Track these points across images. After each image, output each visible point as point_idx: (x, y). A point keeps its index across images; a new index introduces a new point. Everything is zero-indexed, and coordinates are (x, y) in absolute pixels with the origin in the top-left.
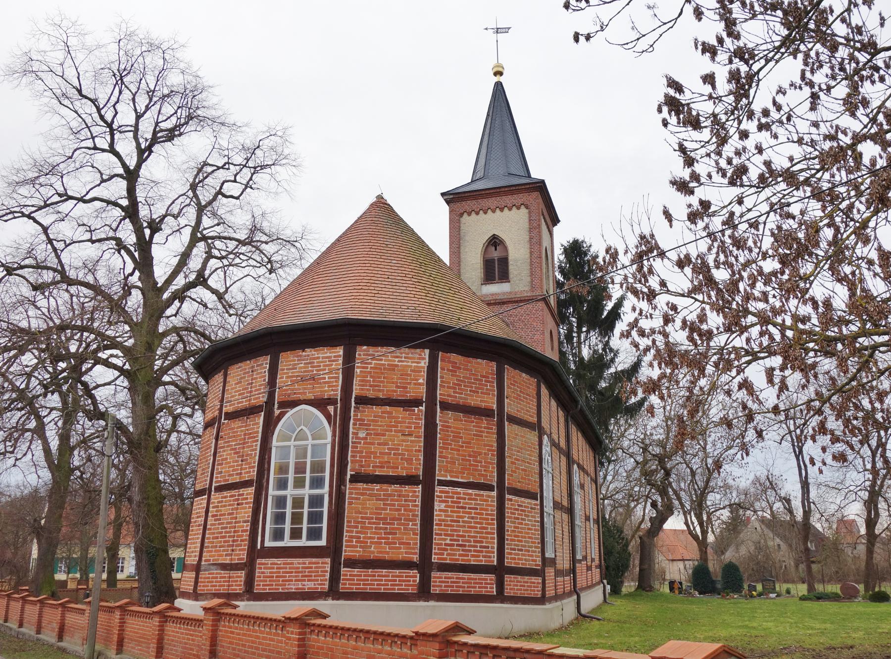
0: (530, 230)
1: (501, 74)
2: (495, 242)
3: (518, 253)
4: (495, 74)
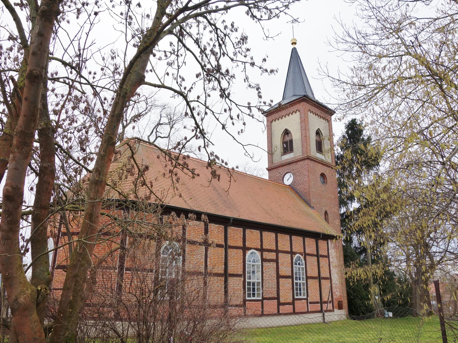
0: (301, 122)
1: (295, 43)
2: (287, 132)
3: (296, 136)
4: (292, 44)
